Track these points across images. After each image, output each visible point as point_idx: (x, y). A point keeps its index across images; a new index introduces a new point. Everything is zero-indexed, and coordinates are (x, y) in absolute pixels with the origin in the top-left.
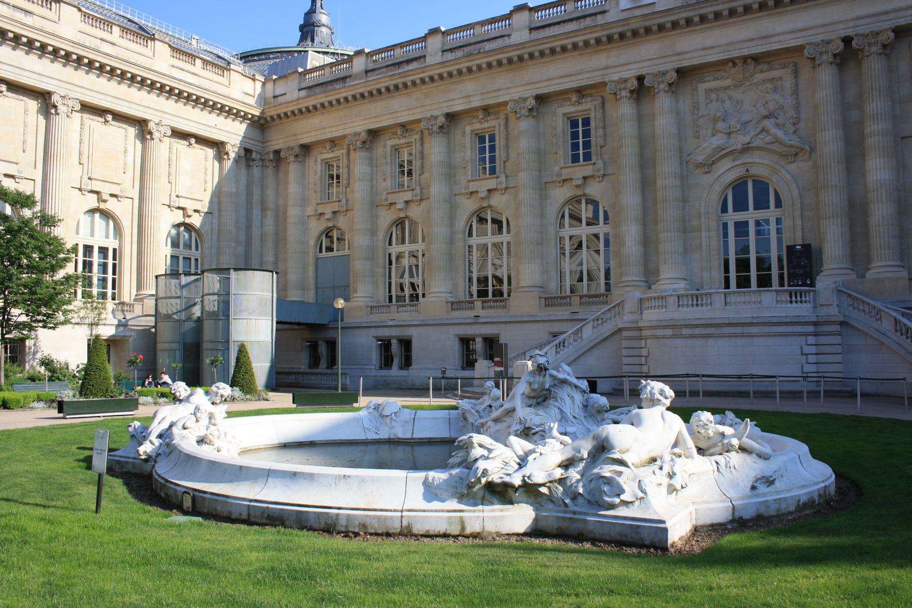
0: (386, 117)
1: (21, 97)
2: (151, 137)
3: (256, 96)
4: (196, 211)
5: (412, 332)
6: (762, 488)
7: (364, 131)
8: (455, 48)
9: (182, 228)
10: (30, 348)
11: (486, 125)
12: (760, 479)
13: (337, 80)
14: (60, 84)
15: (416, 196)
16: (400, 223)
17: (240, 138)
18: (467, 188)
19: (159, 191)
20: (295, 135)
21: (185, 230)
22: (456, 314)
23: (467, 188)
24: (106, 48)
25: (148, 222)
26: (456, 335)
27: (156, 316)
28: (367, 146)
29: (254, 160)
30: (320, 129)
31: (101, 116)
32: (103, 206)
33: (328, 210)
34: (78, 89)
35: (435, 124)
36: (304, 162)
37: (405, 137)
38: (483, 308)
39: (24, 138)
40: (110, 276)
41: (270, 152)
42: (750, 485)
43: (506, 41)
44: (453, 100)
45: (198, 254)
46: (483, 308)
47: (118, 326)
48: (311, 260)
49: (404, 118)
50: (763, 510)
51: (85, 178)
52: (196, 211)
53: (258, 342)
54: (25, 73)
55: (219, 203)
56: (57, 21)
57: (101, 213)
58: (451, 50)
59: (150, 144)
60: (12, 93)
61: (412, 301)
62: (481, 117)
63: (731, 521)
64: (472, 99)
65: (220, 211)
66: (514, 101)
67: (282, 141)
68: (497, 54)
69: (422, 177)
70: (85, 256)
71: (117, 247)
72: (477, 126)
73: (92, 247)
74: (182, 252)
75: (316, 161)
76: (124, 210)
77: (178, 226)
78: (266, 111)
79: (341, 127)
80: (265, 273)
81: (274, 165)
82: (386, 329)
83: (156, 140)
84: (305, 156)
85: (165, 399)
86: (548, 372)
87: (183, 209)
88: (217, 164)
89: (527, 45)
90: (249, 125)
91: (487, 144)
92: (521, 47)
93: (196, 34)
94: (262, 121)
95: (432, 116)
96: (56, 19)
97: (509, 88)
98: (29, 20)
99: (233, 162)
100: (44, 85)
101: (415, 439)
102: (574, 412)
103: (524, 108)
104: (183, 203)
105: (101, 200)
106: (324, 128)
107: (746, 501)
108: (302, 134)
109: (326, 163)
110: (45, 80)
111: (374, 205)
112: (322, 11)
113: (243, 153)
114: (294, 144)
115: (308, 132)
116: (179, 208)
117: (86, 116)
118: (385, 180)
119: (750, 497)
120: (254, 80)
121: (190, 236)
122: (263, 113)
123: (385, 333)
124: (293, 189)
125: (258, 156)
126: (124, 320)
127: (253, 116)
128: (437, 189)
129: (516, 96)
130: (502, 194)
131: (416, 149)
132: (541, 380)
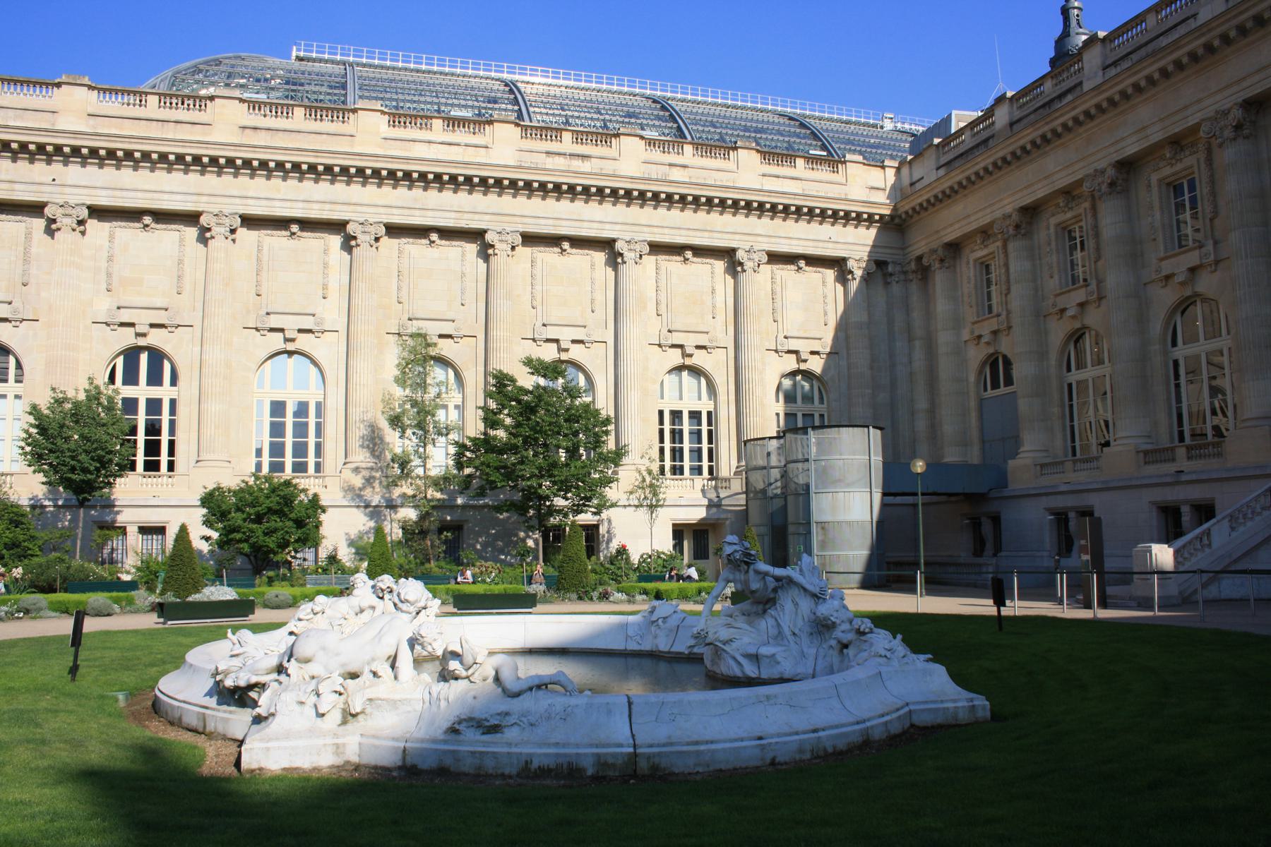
0: (1040, 185)
1: (586, 251)
2: (742, 268)
3: (888, 189)
4: (813, 353)
5: (1093, 500)
6: (471, 735)
7: (1014, 210)
8: (1119, 60)
9: (799, 378)
10: (603, 536)
11: (1179, 167)
12: (465, 720)
13: (977, 146)
14: (625, 227)
15: (1092, 293)
16: (1077, 337)
17: (868, 249)
18: (1158, 271)
19: (759, 335)
20: (937, 232)
21: (802, 379)
22: (1151, 469)
23: (1158, 271)
24: (676, 175)
25: (746, 375)
26: (1153, 503)
27: (746, 493)
28: (1023, 231)
29: (891, 275)
30: (964, 218)
31: (679, 255)
32: (688, 362)
33: (985, 329)
34: (646, 229)
35: (1103, 182)
36: (955, 267)
37: (1071, 209)
38: (1189, 458)
39: (592, 296)
40: (705, 446)
41: (911, 260)
42: (446, 725)
43: (1193, 24)
44: (1123, 139)
45: (823, 408)
46: (1189, 458)
47: (709, 507)
48: (973, 404)
49: (1062, 181)
50: (448, 762)
51: (665, 331)
52: (813, 353)
53: (849, 523)
54: (586, 225)
55: (847, 338)
56: (618, 157)
57: (689, 370)
58: (1115, 64)
59: (742, 277)
60: (576, 248)
61: (675, 474)
62: (1168, 156)
63: (400, 768)
64: (1149, 131)
65: (848, 349)
66: (1209, 119)
67: (923, 243)
68: (1172, 52)
69: (1099, 264)
70: (673, 423)
71: (712, 410)
72: (1167, 171)
73: (681, 412)
74: (800, 407)
75: (968, 263)
76: (717, 364)
77: (793, 374)
78: (899, 206)
79: (988, 211)
80: (856, 429)
81: (920, 277)
82: (1060, 497)
83: (749, 271)
84: (954, 258)
85: (644, 597)
86: (752, 567)
87: (796, 352)
88: (840, 288)
89: (1214, 25)
90: (879, 229)
91: (1187, 196)
92: (1205, 30)
93: (890, 112)
94: (897, 221)
95: (1096, 171)
96: (616, 155)
97: (1199, 101)
98: (586, 166)
99: (860, 282)
100: (606, 234)
101: (672, 653)
102: (795, 626)
103: (1226, 126)
104: (793, 345)
105: (685, 355)
106: (969, 216)
107: (424, 745)
108: (945, 228)
109: (982, 263)
110: (608, 226)
111: (1039, 315)
112: (1081, 30)
113: (874, 268)
114: (934, 245)
115: (951, 225)
116: (789, 352)
117: (661, 258)
118: (1052, 277)
119: (445, 742)
120: (883, 167)
121: (812, 386)
122: (895, 209)
123: (1059, 502)
124: (942, 306)
125: (898, 268)
126: (716, 500)
127: (882, 216)
128: (1115, 279)
129: (1210, 112)
130: (1212, 272)
131: (1086, 223)
132: (742, 577)
